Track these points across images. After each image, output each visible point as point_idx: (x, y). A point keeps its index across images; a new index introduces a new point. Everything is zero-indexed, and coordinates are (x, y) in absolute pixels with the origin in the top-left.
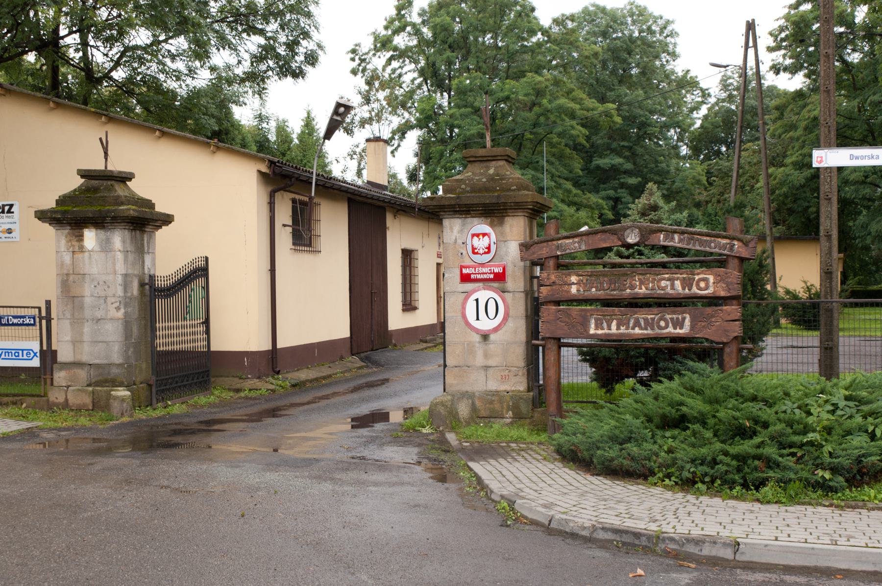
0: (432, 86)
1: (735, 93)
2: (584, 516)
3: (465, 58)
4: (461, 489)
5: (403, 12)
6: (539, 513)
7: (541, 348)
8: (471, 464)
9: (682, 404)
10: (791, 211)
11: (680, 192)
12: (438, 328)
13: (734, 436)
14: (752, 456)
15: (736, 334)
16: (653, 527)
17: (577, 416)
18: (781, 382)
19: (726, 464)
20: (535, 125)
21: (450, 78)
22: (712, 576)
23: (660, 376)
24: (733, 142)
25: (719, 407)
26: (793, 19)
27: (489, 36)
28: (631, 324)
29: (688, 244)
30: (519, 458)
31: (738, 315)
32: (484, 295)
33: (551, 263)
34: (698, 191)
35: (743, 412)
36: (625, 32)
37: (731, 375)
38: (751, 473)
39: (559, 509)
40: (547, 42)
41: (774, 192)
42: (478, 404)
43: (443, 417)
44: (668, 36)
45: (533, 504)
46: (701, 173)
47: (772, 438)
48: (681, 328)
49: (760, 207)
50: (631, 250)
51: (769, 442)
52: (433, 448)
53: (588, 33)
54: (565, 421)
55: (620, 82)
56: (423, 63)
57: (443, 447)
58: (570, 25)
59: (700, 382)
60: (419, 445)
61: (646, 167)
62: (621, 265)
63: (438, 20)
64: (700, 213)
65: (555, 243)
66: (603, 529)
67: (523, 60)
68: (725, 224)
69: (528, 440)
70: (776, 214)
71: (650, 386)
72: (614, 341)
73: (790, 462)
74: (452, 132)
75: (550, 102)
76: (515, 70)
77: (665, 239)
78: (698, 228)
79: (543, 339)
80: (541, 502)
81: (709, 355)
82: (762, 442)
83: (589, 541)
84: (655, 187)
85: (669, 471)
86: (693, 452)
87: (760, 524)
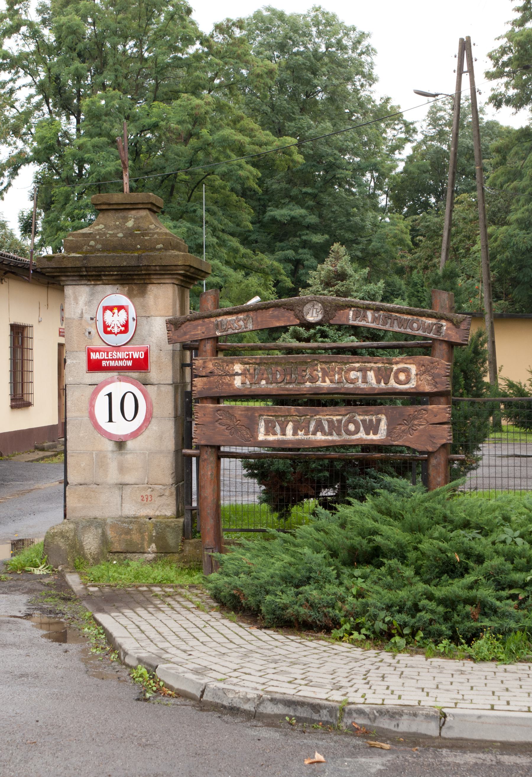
0: (55, 106)
1: (447, 129)
2: (247, 684)
3: (99, 71)
4: (85, 651)
5: (16, 7)
6: (189, 683)
7: (194, 459)
8: (100, 617)
9: (375, 532)
10: (515, 282)
11: (378, 254)
12: (60, 431)
13: (442, 573)
14: (455, 604)
15: (444, 441)
16: (337, 696)
17: (241, 550)
18: (499, 503)
19: (431, 611)
20: (192, 162)
21: (79, 97)
22: (411, 760)
23: (348, 495)
24: (444, 191)
25: (422, 537)
26: (518, 38)
27: (131, 43)
28: (312, 429)
29: (385, 324)
30: (164, 607)
31: (447, 417)
32: (119, 388)
33: (209, 347)
34: (400, 253)
35: (452, 543)
36: (309, 46)
37: (437, 494)
38: (462, 622)
39: (214, 675)
40: (207, 54)
41: (495, 257)
42: (110, 534)
43: (63, 552)
44: (362, 53)
45: (181, 669)
46: (405, 230)
47: (488, 576)
48: (375, 433)
49: (477, 276)
50: (312, 331)
51: (484, 581)
52: (48, 595)
53: (261, 44)
54: (225, 557)
55: (303, 110)
56: (43, 75)
57: (63, 594)
58: (237, 33)
59: (398, 504)
60: (30, 591)
61: (335, 221)
62: (299, 351)
63: (63, 19)
64: (403, 282)
65: (213, 320)
66: (272, 700)
67: (177, 77)
68: (431, 298)
69: (177, 582)
70: (497, 285)
71: (336, 509)
72: (290, 450)
73: (510, 606)
74: (81, 168)
75: (211, 132)
76: (166, 90)
77: (356, 317)
78: (398, 304)
79: (198, 447)
80: (191, 666)
81: (411, 467)
82: (476, 582)
83: (253, 716)
84: (343, 249)
85: (358, 621)
86: (388, 596)
87: (472, 688)
